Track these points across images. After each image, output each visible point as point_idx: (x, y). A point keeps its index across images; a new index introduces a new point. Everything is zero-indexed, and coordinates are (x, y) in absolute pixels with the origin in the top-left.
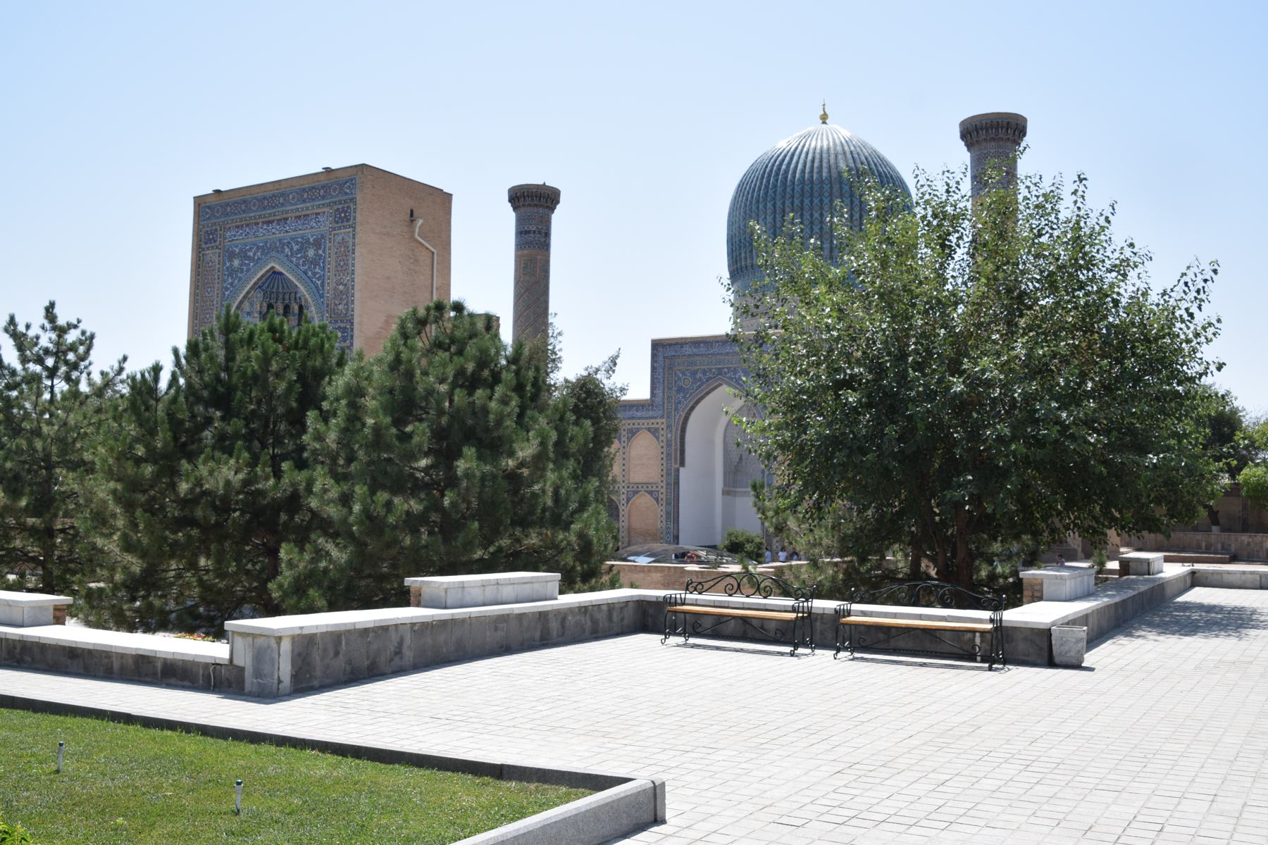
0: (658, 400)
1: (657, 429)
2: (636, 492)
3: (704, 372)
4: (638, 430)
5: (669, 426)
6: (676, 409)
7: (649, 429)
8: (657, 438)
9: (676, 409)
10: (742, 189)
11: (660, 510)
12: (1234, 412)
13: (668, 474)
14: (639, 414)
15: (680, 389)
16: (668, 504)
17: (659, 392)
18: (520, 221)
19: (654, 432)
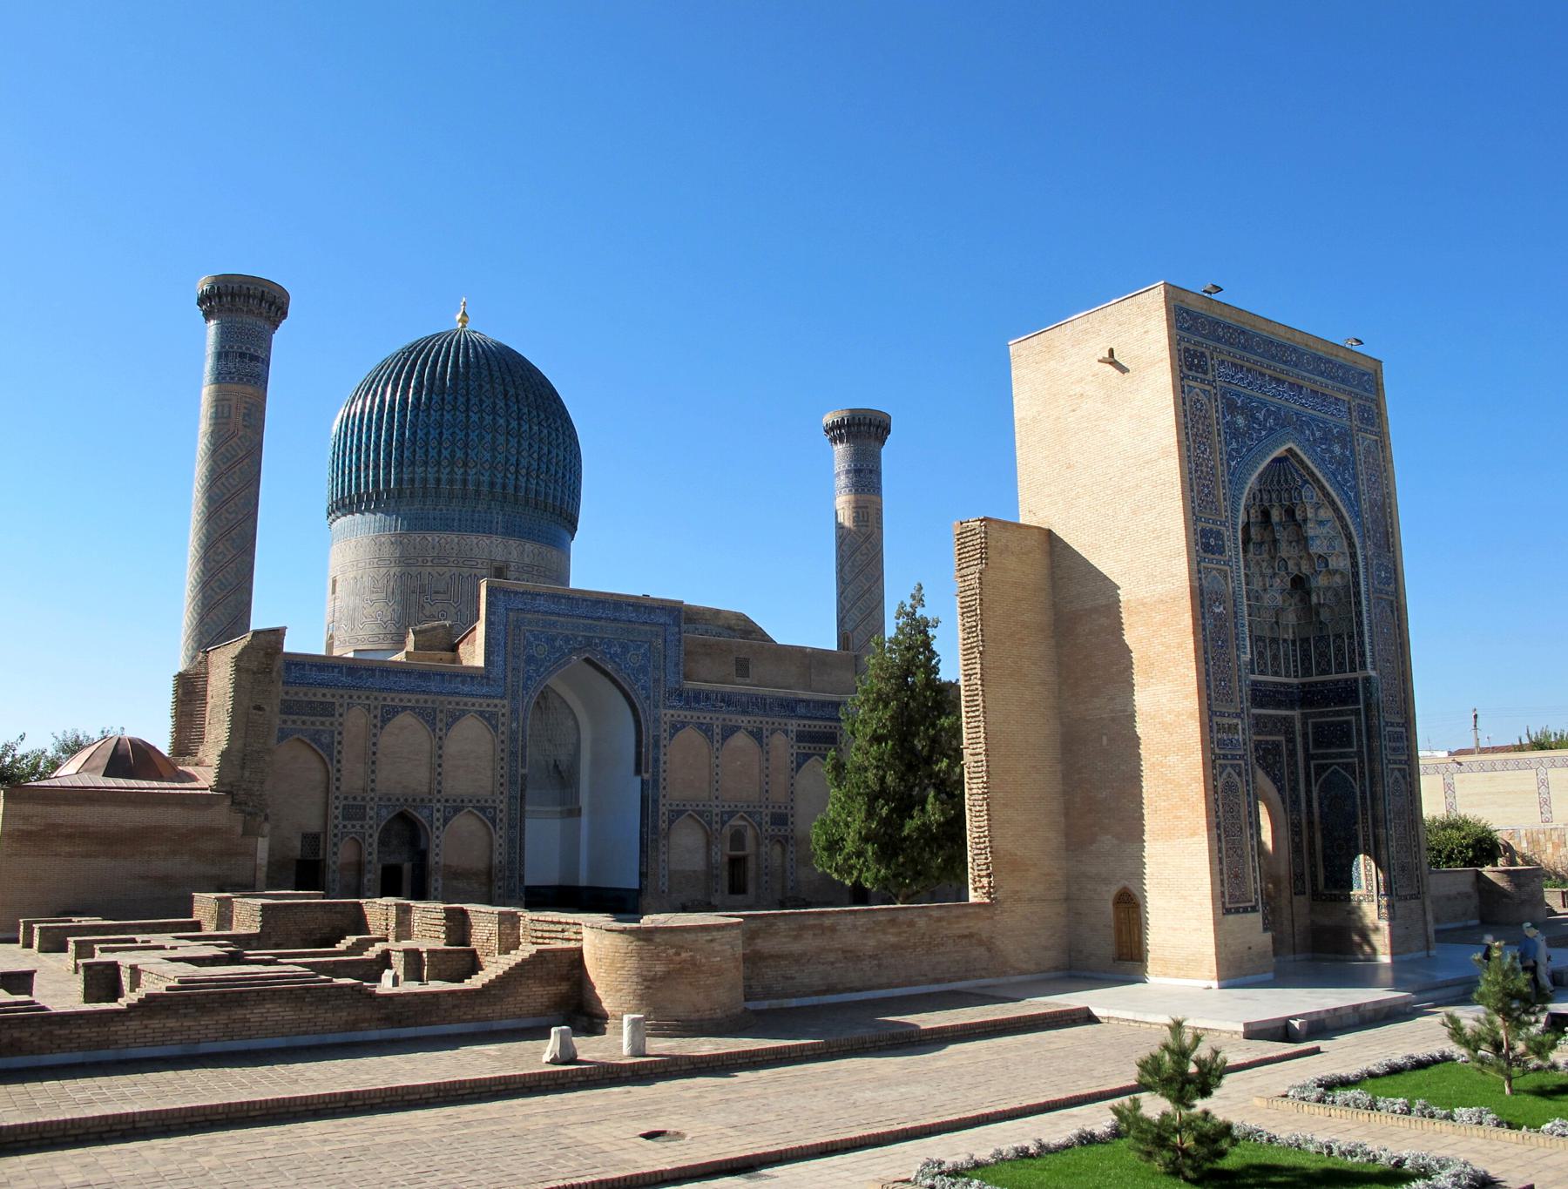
0: (497, 672)
1: (493, 714)
2: (457, 810)
3: (567, 640)
4: (464, 713)
5: (514, 711)
6: (525, 687)
7: (481, 714)
8: (495, 728)
9: (525, 687)
10: (1107, 589)
11: (1348, 562)
12: (1484, 829)
13: (512, 783)
14: (466, 689)
15: (530, 659)
16: (511, 827)
17: (498, 660)
18: (218, 391)
19: (489, 718)
